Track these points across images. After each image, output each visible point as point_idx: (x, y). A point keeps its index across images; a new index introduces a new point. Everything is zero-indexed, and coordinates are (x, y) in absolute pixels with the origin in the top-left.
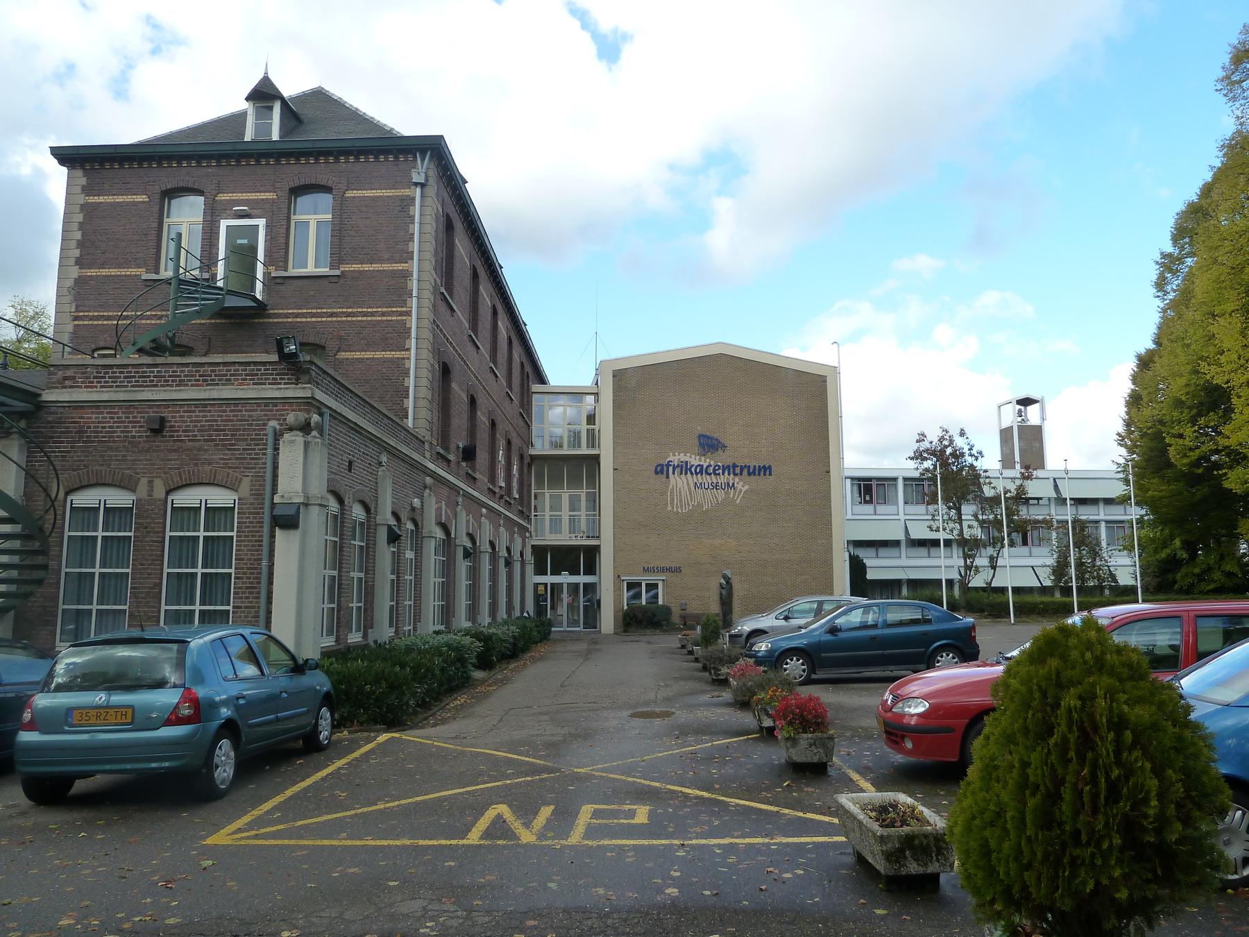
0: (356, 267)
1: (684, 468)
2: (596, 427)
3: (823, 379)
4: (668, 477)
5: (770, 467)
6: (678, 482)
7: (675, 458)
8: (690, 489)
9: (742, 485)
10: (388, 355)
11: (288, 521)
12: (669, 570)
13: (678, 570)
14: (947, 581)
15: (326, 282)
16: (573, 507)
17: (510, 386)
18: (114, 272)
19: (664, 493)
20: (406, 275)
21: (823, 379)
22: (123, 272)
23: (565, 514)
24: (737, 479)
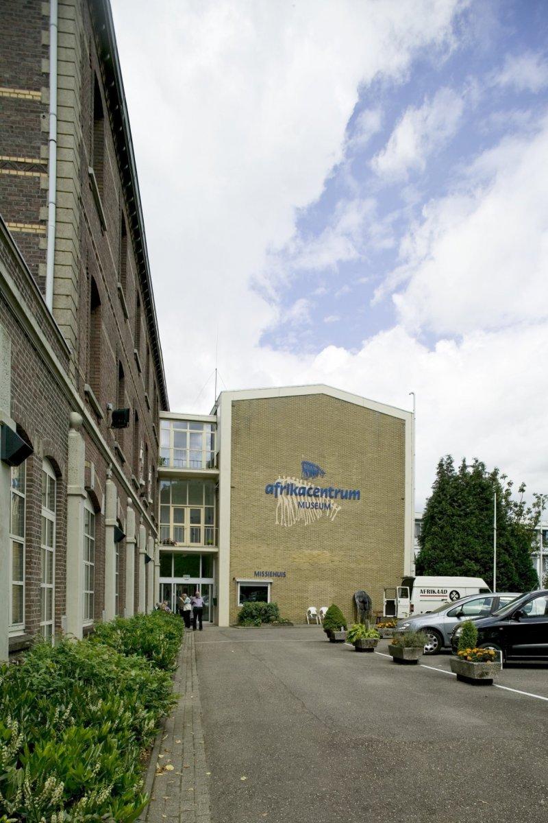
1: (290, 490)
3: (402, 423)
4: (276, 496)
5: (359, 493)
6: (285, 501)
7: (283, 481)
9: (336, 506)
12: (276, 574)
13: (284, 575)
21: (402, 423)
23: (187, 524)
24: (332, 501)
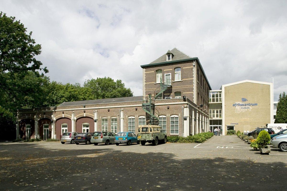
0: (185, 79)
1: (239, 105)
2: (221, 98)
5: (257, 104)
6: (238, 108)
7: (237, 103)
8: (240, 109)
9: (251, 107)
10: (190, 92)
11: (185, 119)
14: (211, 124)
15: (180, 82)
16: (217, 112)
17: (204, 89)
18: (150, 83)
19: (235, 109)
20: (193, 80)
22: (152, 83)
23: (215, 114)
24: (250, 106)
